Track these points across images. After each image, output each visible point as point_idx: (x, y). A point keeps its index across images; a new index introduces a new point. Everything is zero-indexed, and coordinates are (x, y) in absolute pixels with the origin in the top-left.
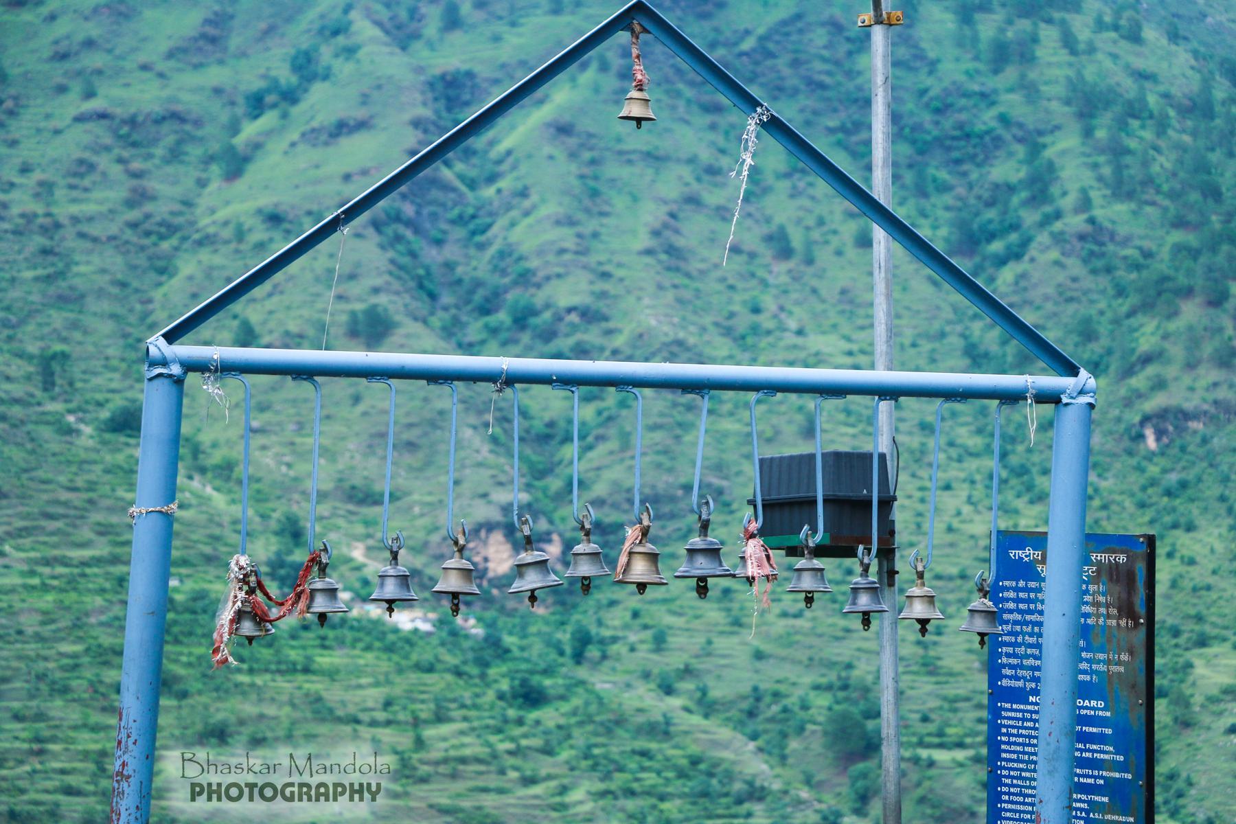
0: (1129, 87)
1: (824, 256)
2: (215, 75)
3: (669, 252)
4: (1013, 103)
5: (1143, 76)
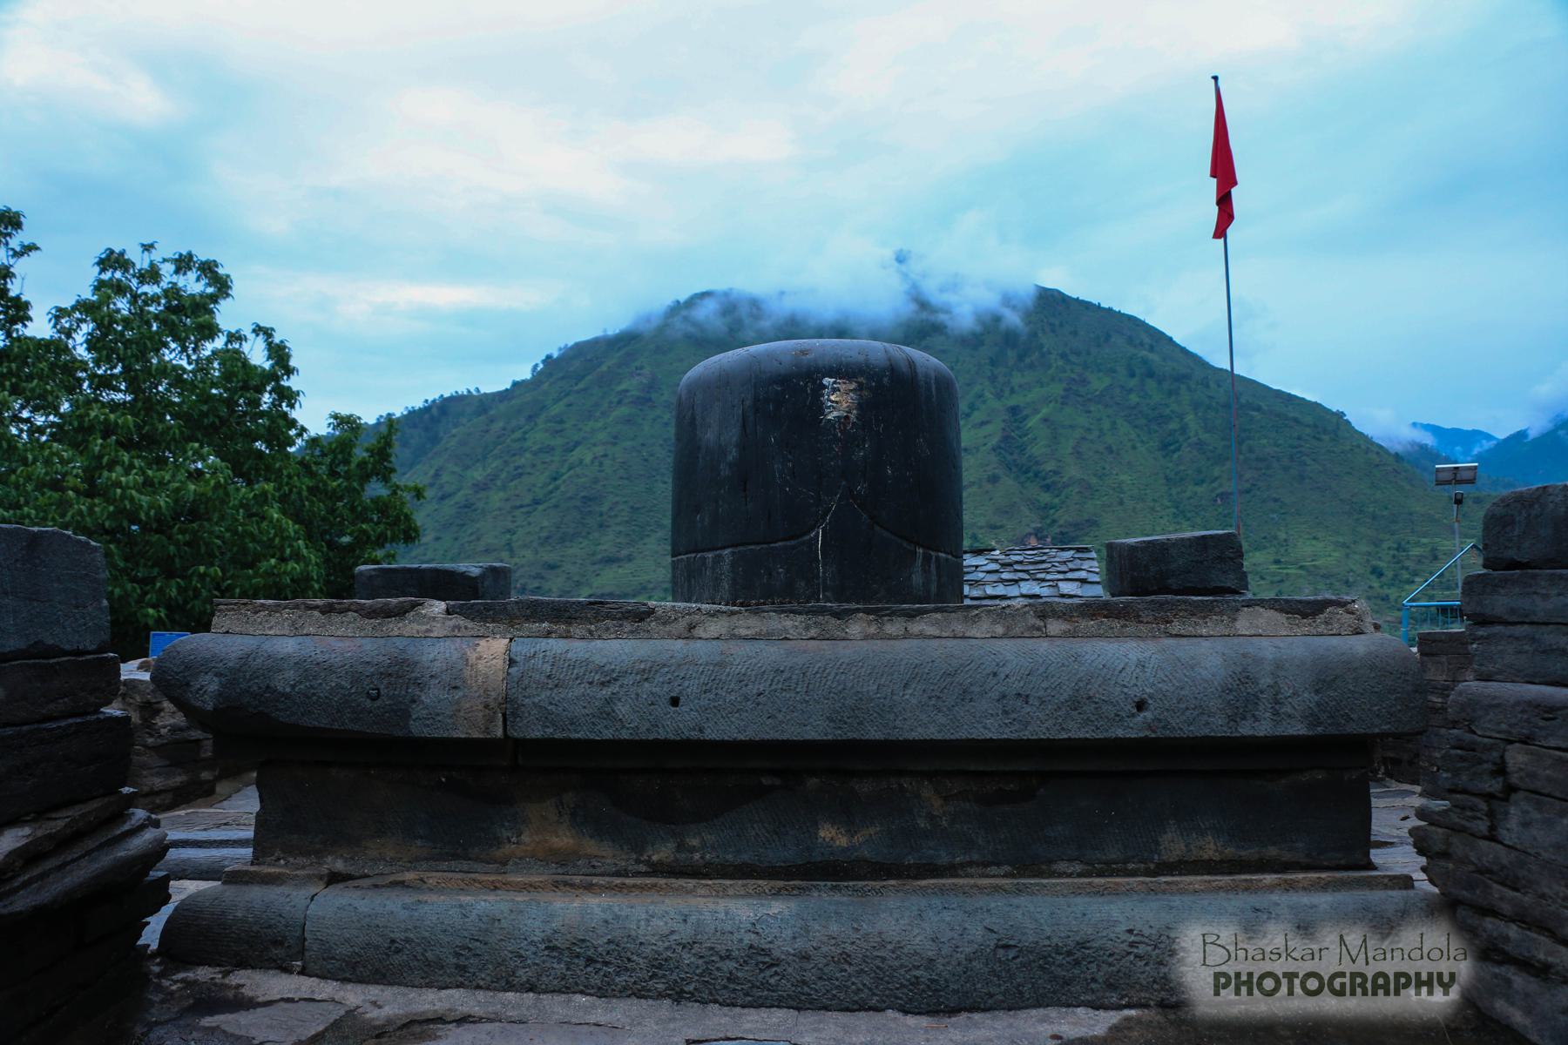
3: (1077, 453)
5: (1211, 398)
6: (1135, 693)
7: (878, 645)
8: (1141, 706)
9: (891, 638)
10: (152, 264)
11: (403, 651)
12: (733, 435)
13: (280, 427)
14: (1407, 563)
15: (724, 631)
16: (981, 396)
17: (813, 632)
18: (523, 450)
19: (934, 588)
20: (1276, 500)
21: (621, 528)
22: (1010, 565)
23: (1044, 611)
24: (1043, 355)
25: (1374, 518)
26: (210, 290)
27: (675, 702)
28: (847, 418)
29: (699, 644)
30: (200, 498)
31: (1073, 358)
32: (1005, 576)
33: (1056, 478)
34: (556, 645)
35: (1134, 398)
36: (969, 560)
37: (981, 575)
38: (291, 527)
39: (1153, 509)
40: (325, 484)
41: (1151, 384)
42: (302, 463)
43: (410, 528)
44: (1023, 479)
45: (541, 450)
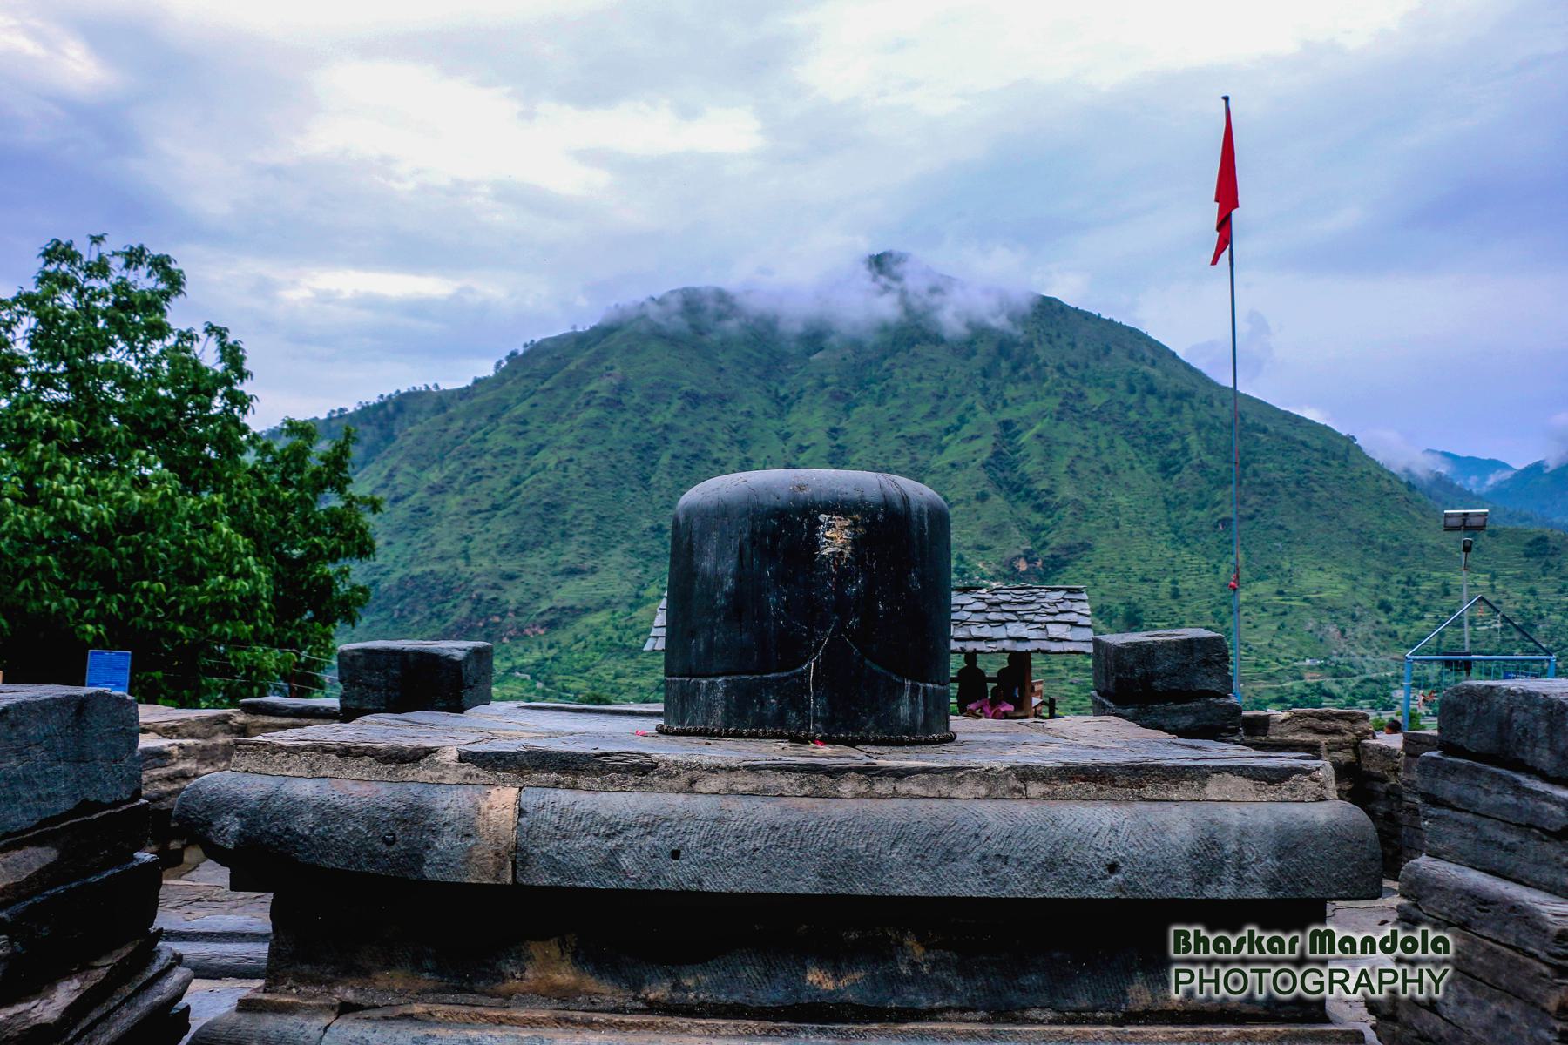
0: (1211, 421)
1: (1120, 472)
2: (937, 423)
3: (1072, 472)
4: (1176, 426)
6: (1108, 856)
7: (868, 804)
8: (1113, 868)
9: (880, 797)
10: (101, 258)
11: (418, 798)
12: (730, 565)
13: (229, 436)
14: (1417, 598)
15: (722, 786)
16: (972, 408)
17: (807, 790)
18: (481, 453)
19: (920, 718)
20: (1280, 528)
21: (586, 538)
22: (997, 605)
23: (1026, 774)
24: (1038, 368)
25: (1384, 549)
26: (162, 286)
27: (676, 855)
28: (841, 554)
29: (700, 798)
30: (146, 508)
31: (1070, 371)
32: (992, 616)
33: (1049, 498)
34: (564, 797)
35: (1133, 416)
36: (956, 598)
37: (967, 615)
38: (241, 542)
39: (1150, 534)
40: (277, 494)
41: (1152, 401)
42: (253, 471)
43: (365, 542)
44: (1013, 498)
45: (502, 453)
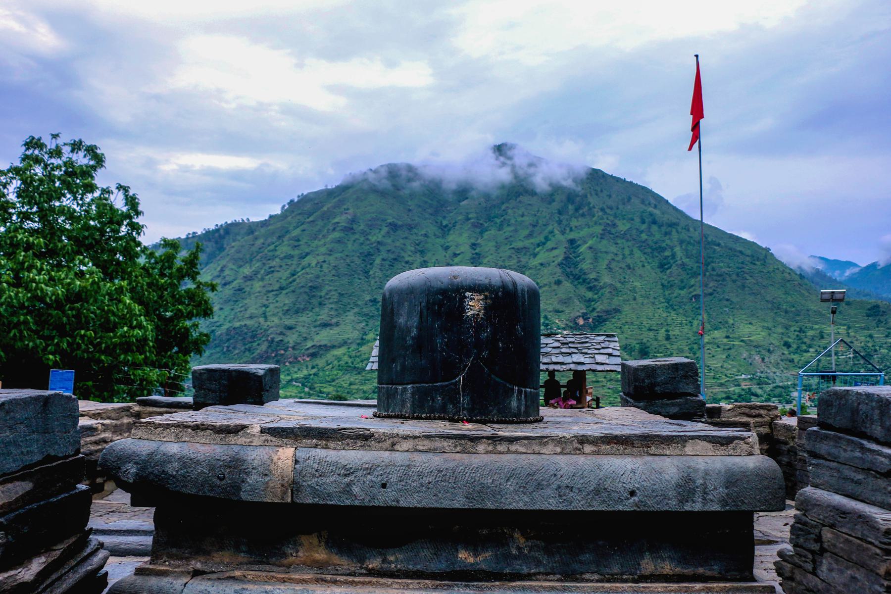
0: (688, 239)
1: (636, 268)
2: (532, 240)
3: (609, 268)
4: (668, 242)
6: (630, 487)
7: (493, 457)
8: (632, 493)
9: (500, 453)
10: (57, 146)
11: (238, 453)
12: (415, 321)
13: (130, 248)
14: (805, 340)
15: (411, 447)
16: (552, 232)
17: (458, 449)
18: (273, 258)
19: (523, 408)
20: (728, 300)
21: (333, 306)
22: (567, 344)
23: (583, 440)
24: (590, 209)
25: (786, 312)
26: (92, 163)
27: (384, 486)
28: (478, 315)
29: (398, 454)
30: (83, 289)
31: (608, 211)
32: (563, 350)
33: (596, 283)
34: (320, 453)
35: (644, 236)
36: (543, 340)
37: (549, 349)
38: (137, 308)
39: (653, 303)
40: (157, 281)
41: (655, 228)
42: (143, 268)
43: (207, 308)
44: (576, 283)
45: (285, 257)
